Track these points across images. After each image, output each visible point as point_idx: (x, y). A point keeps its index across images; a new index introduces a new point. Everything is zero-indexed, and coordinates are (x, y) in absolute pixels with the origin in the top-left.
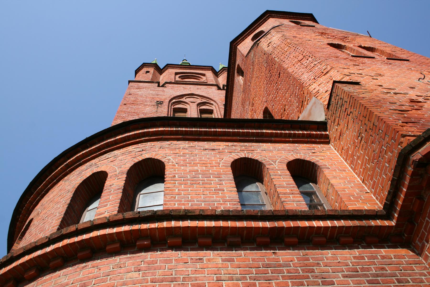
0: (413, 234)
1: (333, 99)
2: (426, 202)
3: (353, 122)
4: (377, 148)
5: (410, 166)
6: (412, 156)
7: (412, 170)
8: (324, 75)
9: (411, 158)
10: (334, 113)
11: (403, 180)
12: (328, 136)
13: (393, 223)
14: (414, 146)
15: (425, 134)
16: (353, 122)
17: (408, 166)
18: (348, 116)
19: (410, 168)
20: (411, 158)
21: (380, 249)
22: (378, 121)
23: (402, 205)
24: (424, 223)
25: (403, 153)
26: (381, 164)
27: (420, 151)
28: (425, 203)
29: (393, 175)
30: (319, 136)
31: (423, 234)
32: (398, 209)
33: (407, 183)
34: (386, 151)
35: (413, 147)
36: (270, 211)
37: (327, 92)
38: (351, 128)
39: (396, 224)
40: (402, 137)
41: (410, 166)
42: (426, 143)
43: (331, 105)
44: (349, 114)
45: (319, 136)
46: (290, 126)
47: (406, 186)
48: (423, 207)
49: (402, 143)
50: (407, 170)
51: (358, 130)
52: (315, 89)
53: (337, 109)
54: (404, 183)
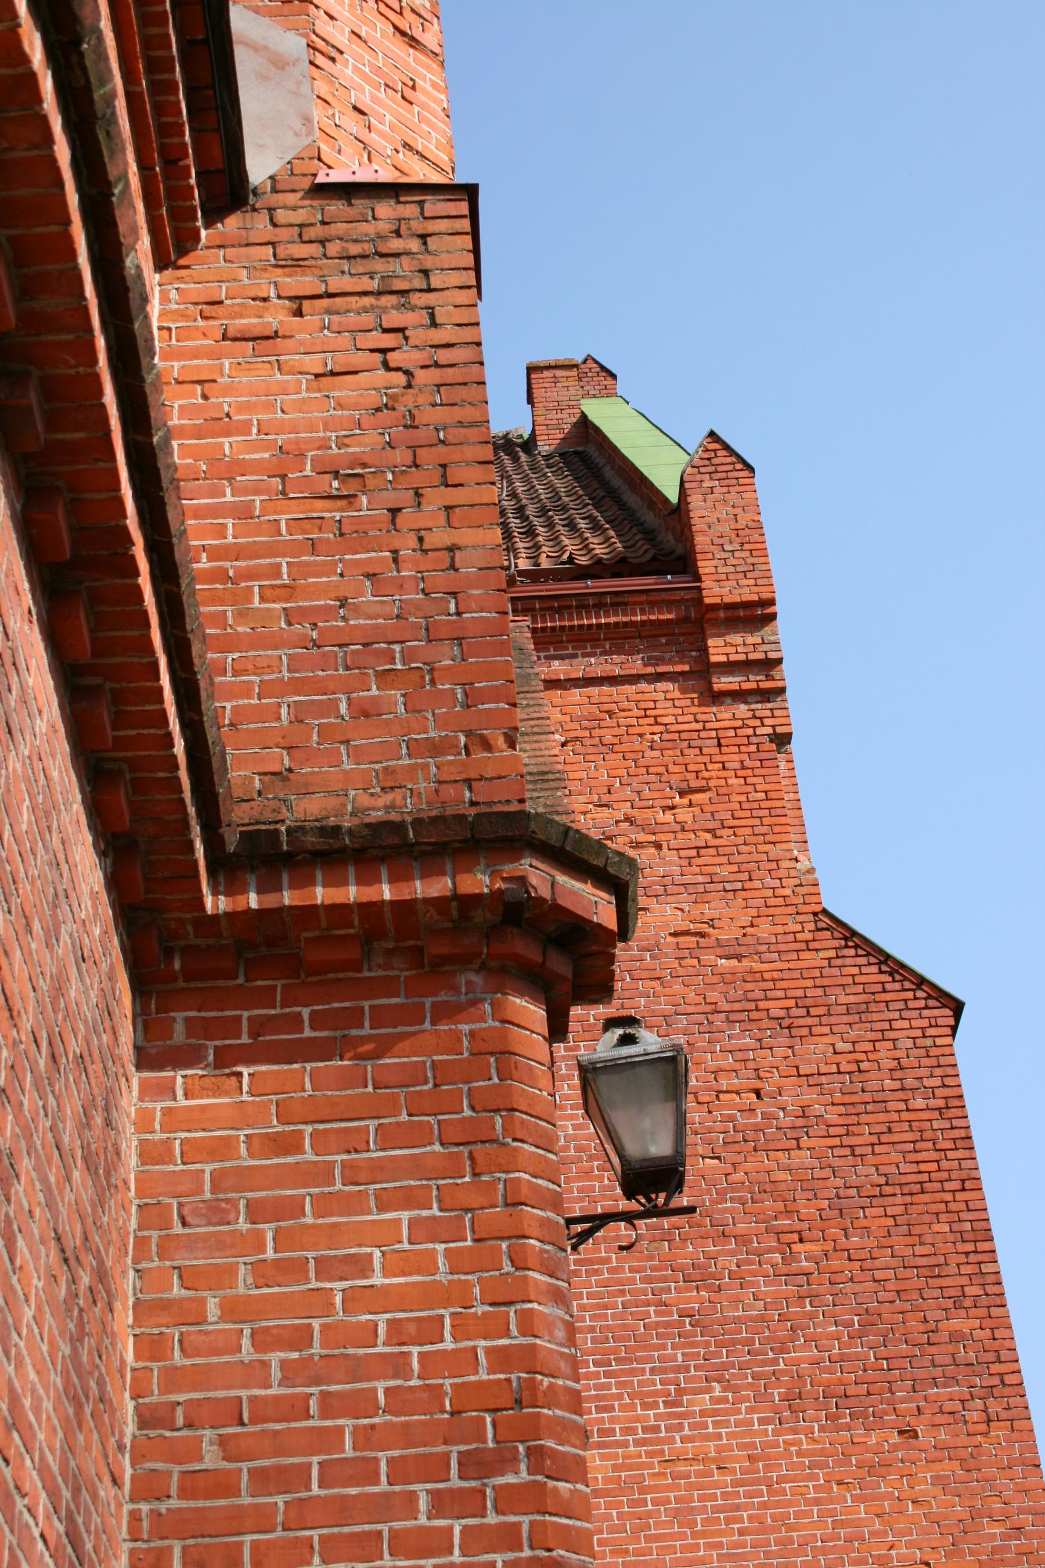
0: (193, 985)
1: (386, 209)
2: (359, 975)
3: (378, 410)
4: (370, 618)
5: (493, 872)
6: (535, 863)
7: (486, 890)
8: (395, 27)
9: (526, 861)
10: (322, 242)
11: (415, 864)
12: (189, 245)
13: (214, 903)
14: (568, 849)
15: (617, 859)
16: (378, 410)
17: (488, 866)
18: (378, 357)
19: (487, 880)
20: (523, 862)
21: (315, 1038)
22: (480, 569)
23: (315, 906)
24: (274, 1007)
25: (533, 826)
26: (320, 673)
27: (562, 879)
28: (351, 974)
29: (417, 822)
30: (180, 203)
31: (232, 1027)
32: (287, 898)
33: (420, 889)
34: (392, 676)
35: (563, 847)
36: (173, 468)
37: (356, 114)
38: (340, 406)
39: (215, 917)
40: (505, 734)
41: (493, 872)
42: (586, 883)
43: (350, 205)
44: (394, 358)
45: (180, 203)
46: (201, 37)
47: (407, 891)
48: (332, 976)
49: (486, 745)
50: (469, 870)
51: (367, 459)
52: (332, 18)
53: (360, 267)
54: (410, 878)
